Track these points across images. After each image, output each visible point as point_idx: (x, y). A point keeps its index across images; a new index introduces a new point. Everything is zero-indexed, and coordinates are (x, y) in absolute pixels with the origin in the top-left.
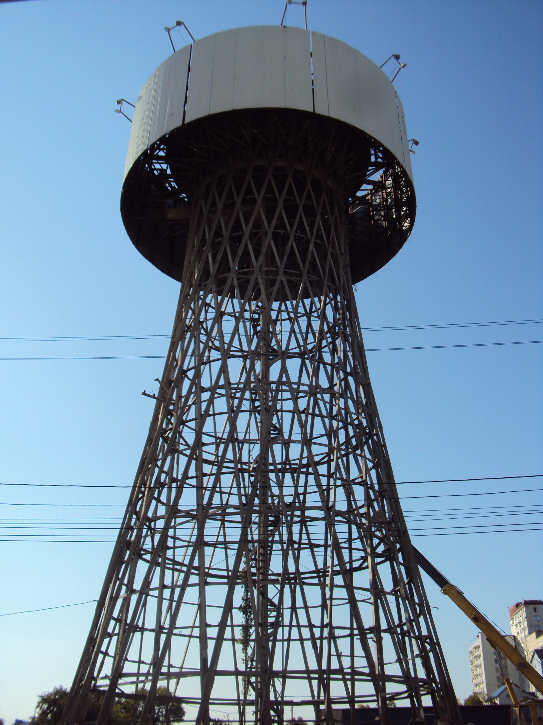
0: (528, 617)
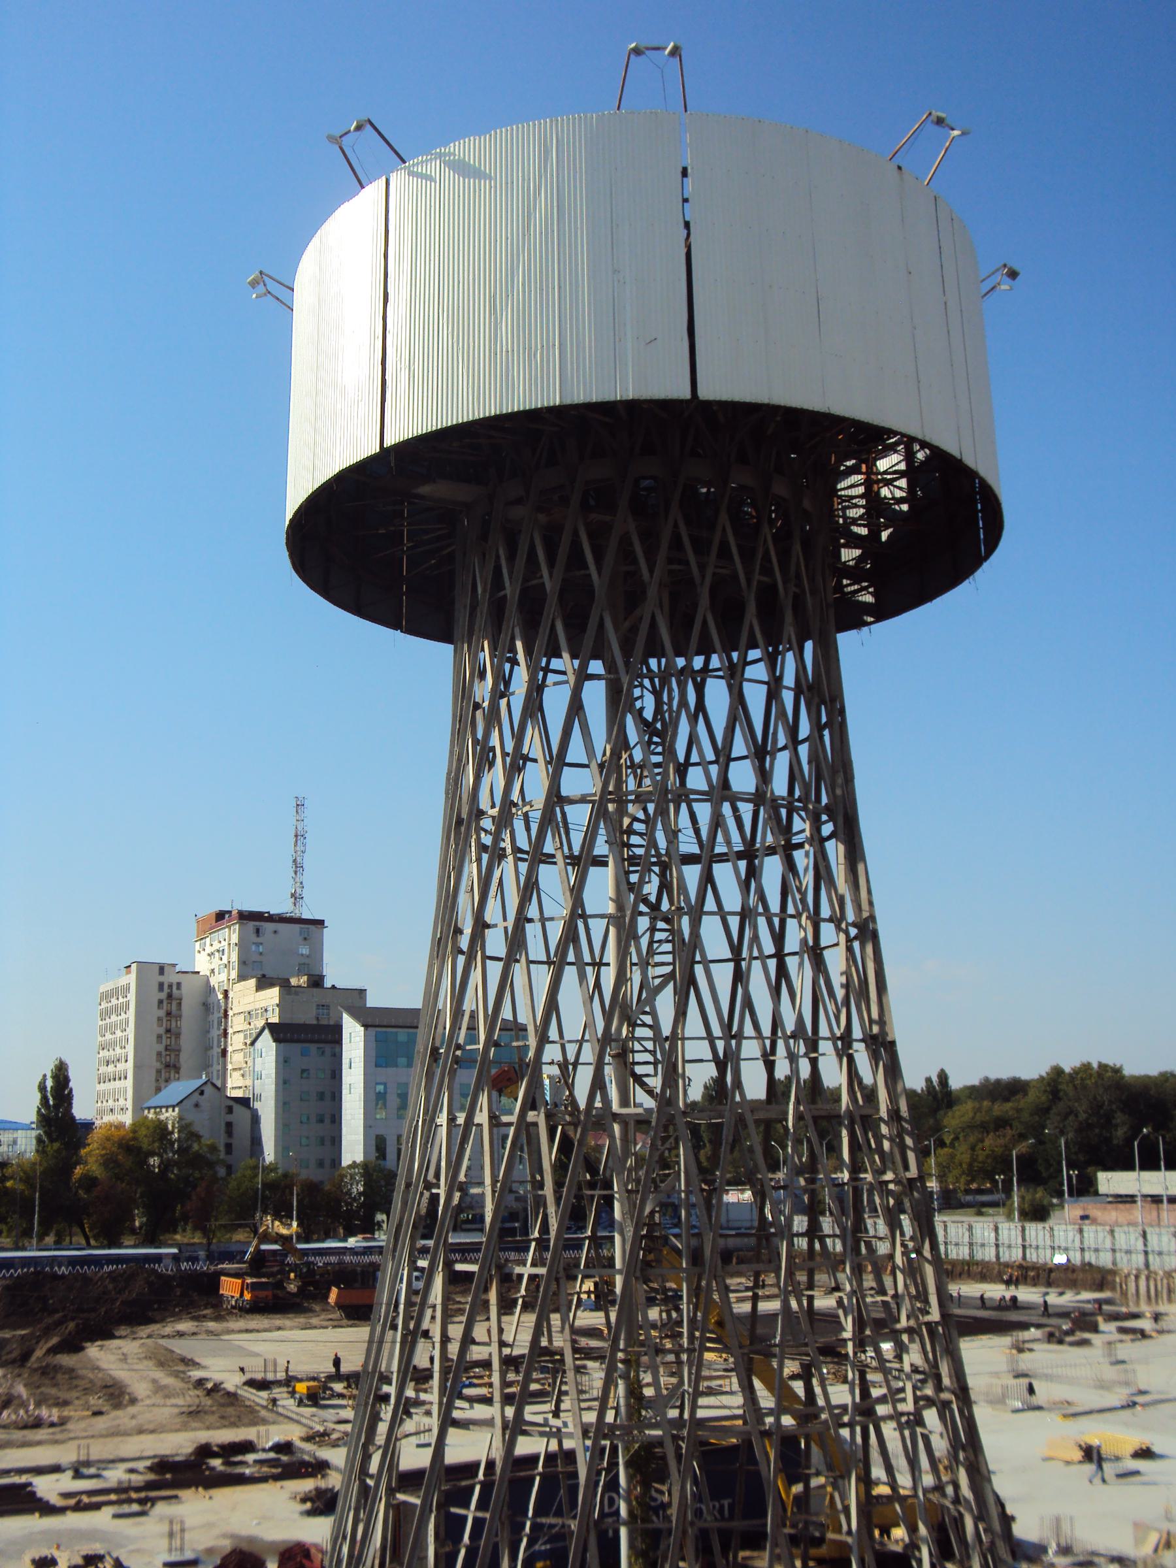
0: (242, 945)
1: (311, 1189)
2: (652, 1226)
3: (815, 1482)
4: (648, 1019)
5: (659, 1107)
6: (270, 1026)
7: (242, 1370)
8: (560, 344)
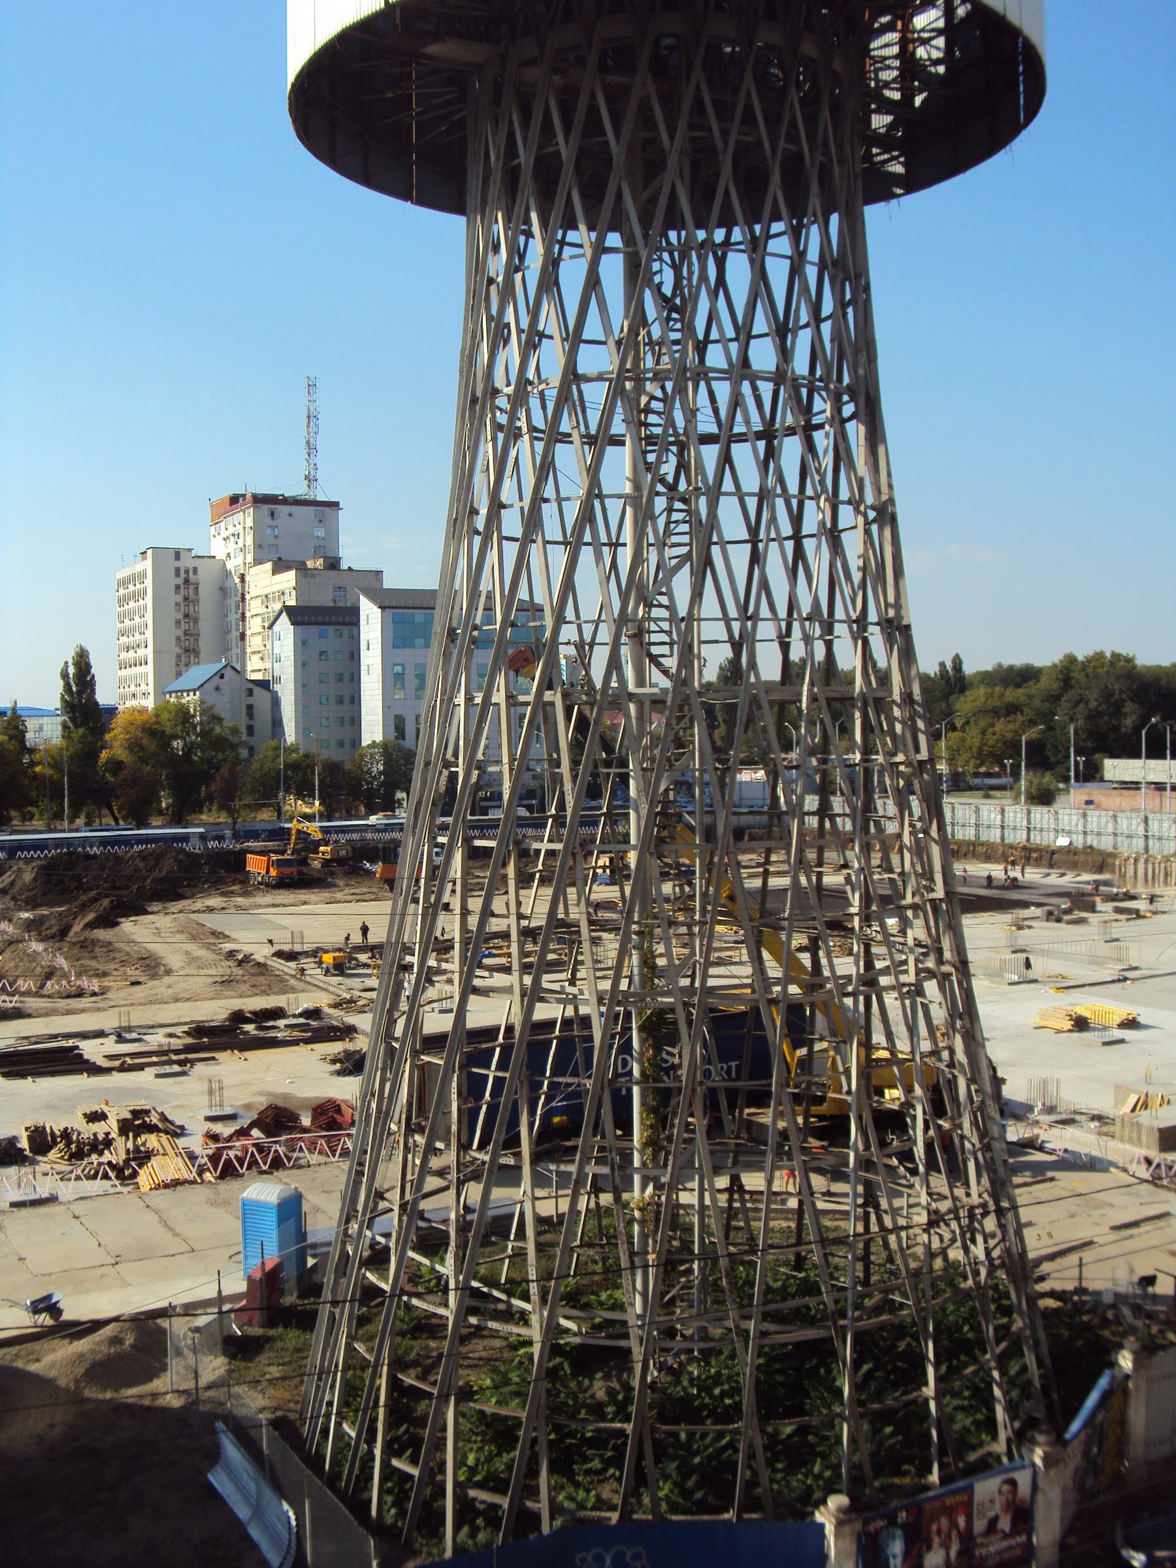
1: (333, 768)
2: (666, 803)
3: (818, 1047)
4: (664, 600)
5: (675, 688)
6: (288, 610)
7: (270, 941)
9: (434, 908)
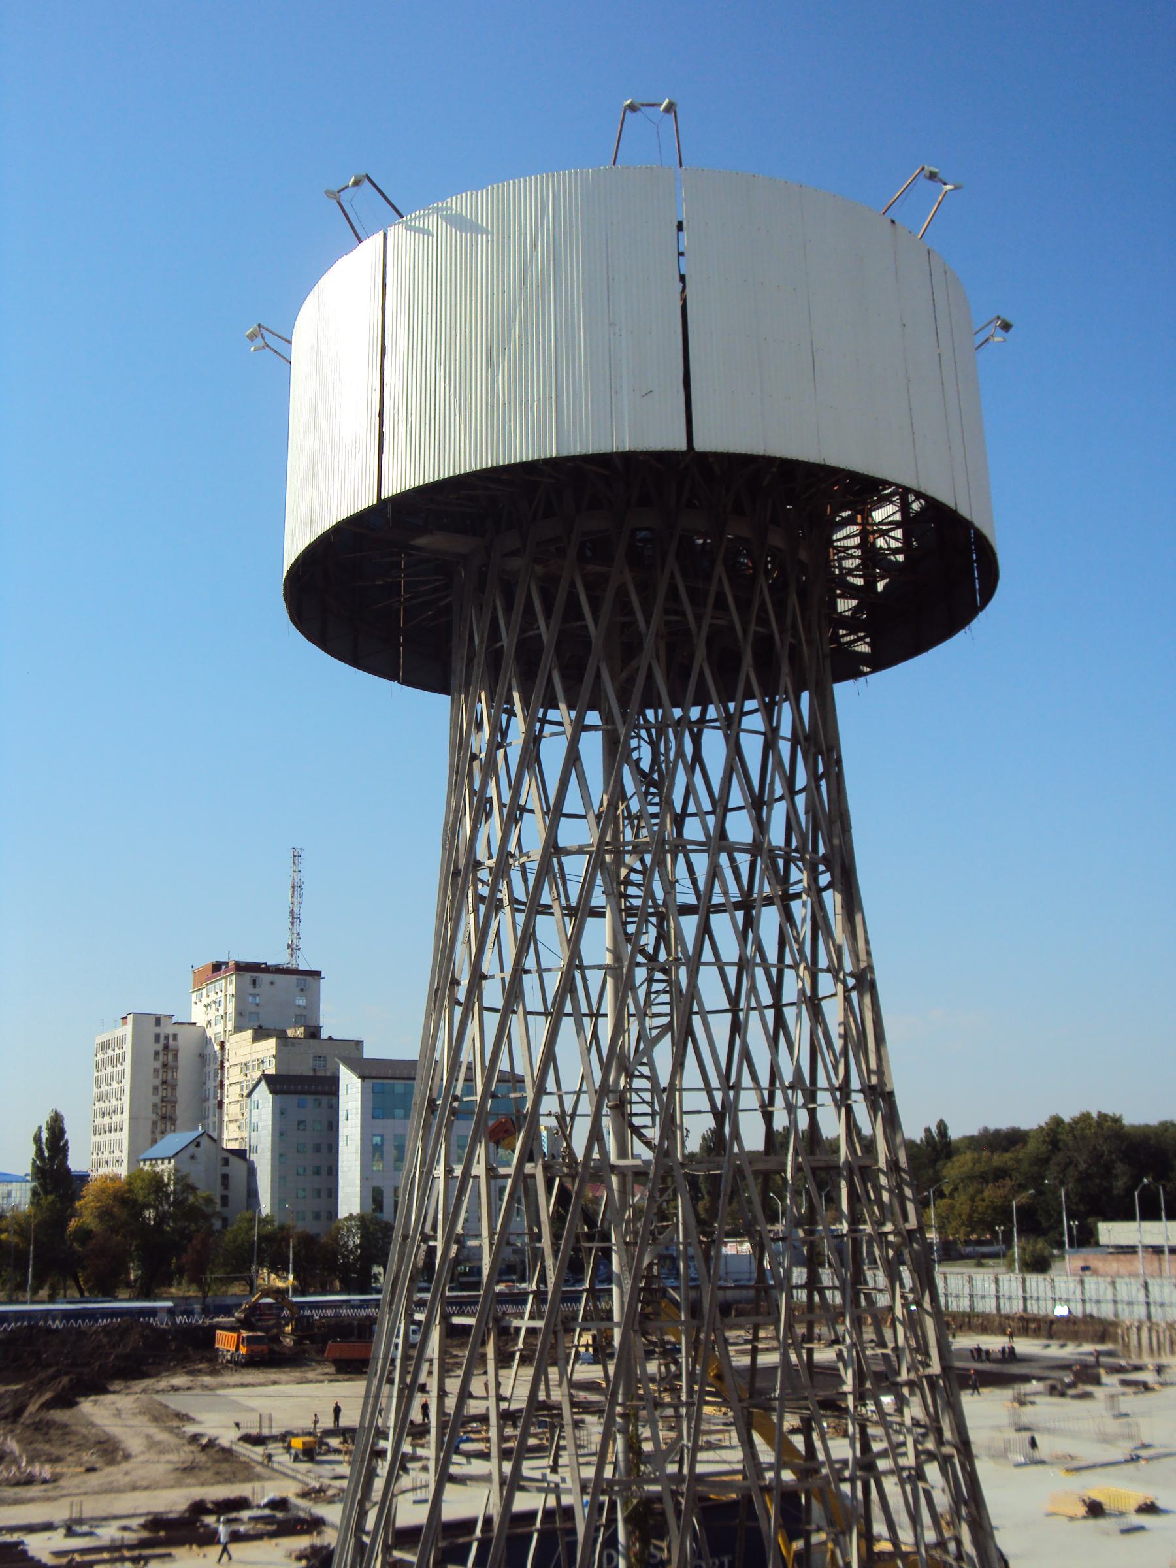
0: (239, 996)
1: (308, 1242)
2: (650, 1278)
3: (816, 1538)
4: (645, 1070)
5: (657, 1159)
6: (268, 1078)
7: (237, 1425)
8: (557, 397)
9: (410, 1389)
